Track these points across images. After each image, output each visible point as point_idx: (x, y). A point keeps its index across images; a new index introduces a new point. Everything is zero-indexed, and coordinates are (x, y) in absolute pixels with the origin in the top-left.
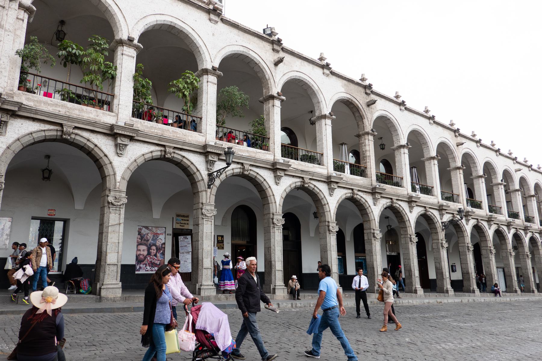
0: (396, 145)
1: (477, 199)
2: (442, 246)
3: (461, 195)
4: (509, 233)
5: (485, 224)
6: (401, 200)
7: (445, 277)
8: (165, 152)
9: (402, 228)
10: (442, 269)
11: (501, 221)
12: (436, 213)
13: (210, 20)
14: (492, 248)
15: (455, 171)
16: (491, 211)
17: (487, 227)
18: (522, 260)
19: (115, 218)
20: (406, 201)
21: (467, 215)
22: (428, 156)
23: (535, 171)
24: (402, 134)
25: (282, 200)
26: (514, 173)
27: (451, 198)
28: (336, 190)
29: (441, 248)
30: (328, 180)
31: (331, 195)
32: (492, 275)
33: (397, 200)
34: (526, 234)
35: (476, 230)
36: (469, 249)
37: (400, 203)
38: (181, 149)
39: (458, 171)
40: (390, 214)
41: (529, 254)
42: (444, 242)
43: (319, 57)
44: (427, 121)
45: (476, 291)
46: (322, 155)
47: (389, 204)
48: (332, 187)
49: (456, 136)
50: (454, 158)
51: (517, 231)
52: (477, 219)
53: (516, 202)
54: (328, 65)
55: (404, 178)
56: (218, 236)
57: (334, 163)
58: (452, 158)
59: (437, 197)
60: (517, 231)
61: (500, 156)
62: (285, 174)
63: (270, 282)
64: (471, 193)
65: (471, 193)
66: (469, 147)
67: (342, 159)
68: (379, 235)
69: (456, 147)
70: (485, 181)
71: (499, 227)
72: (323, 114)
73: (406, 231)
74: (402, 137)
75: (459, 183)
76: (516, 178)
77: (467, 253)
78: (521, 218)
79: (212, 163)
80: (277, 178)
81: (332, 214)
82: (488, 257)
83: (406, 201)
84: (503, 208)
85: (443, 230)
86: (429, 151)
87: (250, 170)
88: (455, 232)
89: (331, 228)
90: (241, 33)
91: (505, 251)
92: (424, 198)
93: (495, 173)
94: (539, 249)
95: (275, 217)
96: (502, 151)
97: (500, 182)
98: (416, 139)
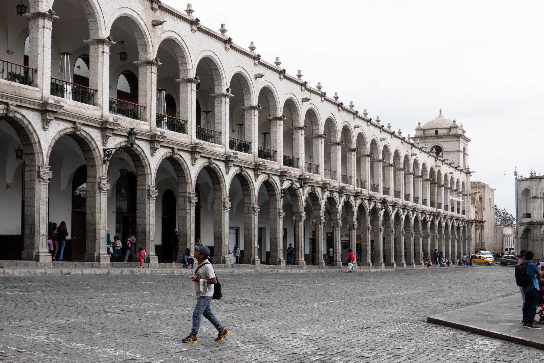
0: (32, 11)
2: (225, 207)
3: (148, 107)
4: (227, 173)
5: (221, 166)
6: (28, 108)
7: (98, 237)
9: (28, 154)
10: (95, 224)
11: (214, 154)
12: (95, 135)
14: (153, 189)
15: (144, 68)
16: (198, 137)
18: (246, 216)
20: (37, 110)
22: (95, 38)
23: (291, 80)
24: (191, 63)
26: (253, 79)
29: (97, 191)
30: (42, 107)
31: (193, 165)
32: (186, 236)
33: (18, 106)
34: (257, 176)
35: (266, 187)
36: (254, 211)
37: (24, 112)
39: (149, 67)
40: (170, 168)
41: (256, 206)
42: (227, 201)
44: (299, 86)
45: (256, 262)
46: (36, 71)
47: (168, 155)
48: (48, 117)
49: (152, 8)
50: (145, 45)
51: (242, 170)
52: (173, 149)
53: (250, 126)
55: (39, 71)
56: (327, 233)
57: (52, 84)
58: (142, 45)
59: (101, 107)
60: (242, 170)
61: (232, 51)
62: (113, 134)
65: (172, 104)
66: (271, 79)
67: (63, 76)
68: (106, 185)
69: (150, 27)
70: (325, 141)
71: (210, 163)
72: (189, 77)
73: (33, 160)
74: (151, 50)
75: (149, 88)
76: (303, 109)
77: (147, 201)
78: (253, 151)
80: (46, 122)
81: (45, 157)
82: (185, 209)
83: (147, 141)
84: (320, 167)
85: (105, 162)
86: (97, 29)
87: (16, 112)
88: (175, 176)
89: (41, 174)
91: (274, 210)
92: (172, 135)
93: (219, 77)
94: (276, 201)
95: (41, 170)
96: (288, 73)
97: (224, 91)
98: (208, 68)
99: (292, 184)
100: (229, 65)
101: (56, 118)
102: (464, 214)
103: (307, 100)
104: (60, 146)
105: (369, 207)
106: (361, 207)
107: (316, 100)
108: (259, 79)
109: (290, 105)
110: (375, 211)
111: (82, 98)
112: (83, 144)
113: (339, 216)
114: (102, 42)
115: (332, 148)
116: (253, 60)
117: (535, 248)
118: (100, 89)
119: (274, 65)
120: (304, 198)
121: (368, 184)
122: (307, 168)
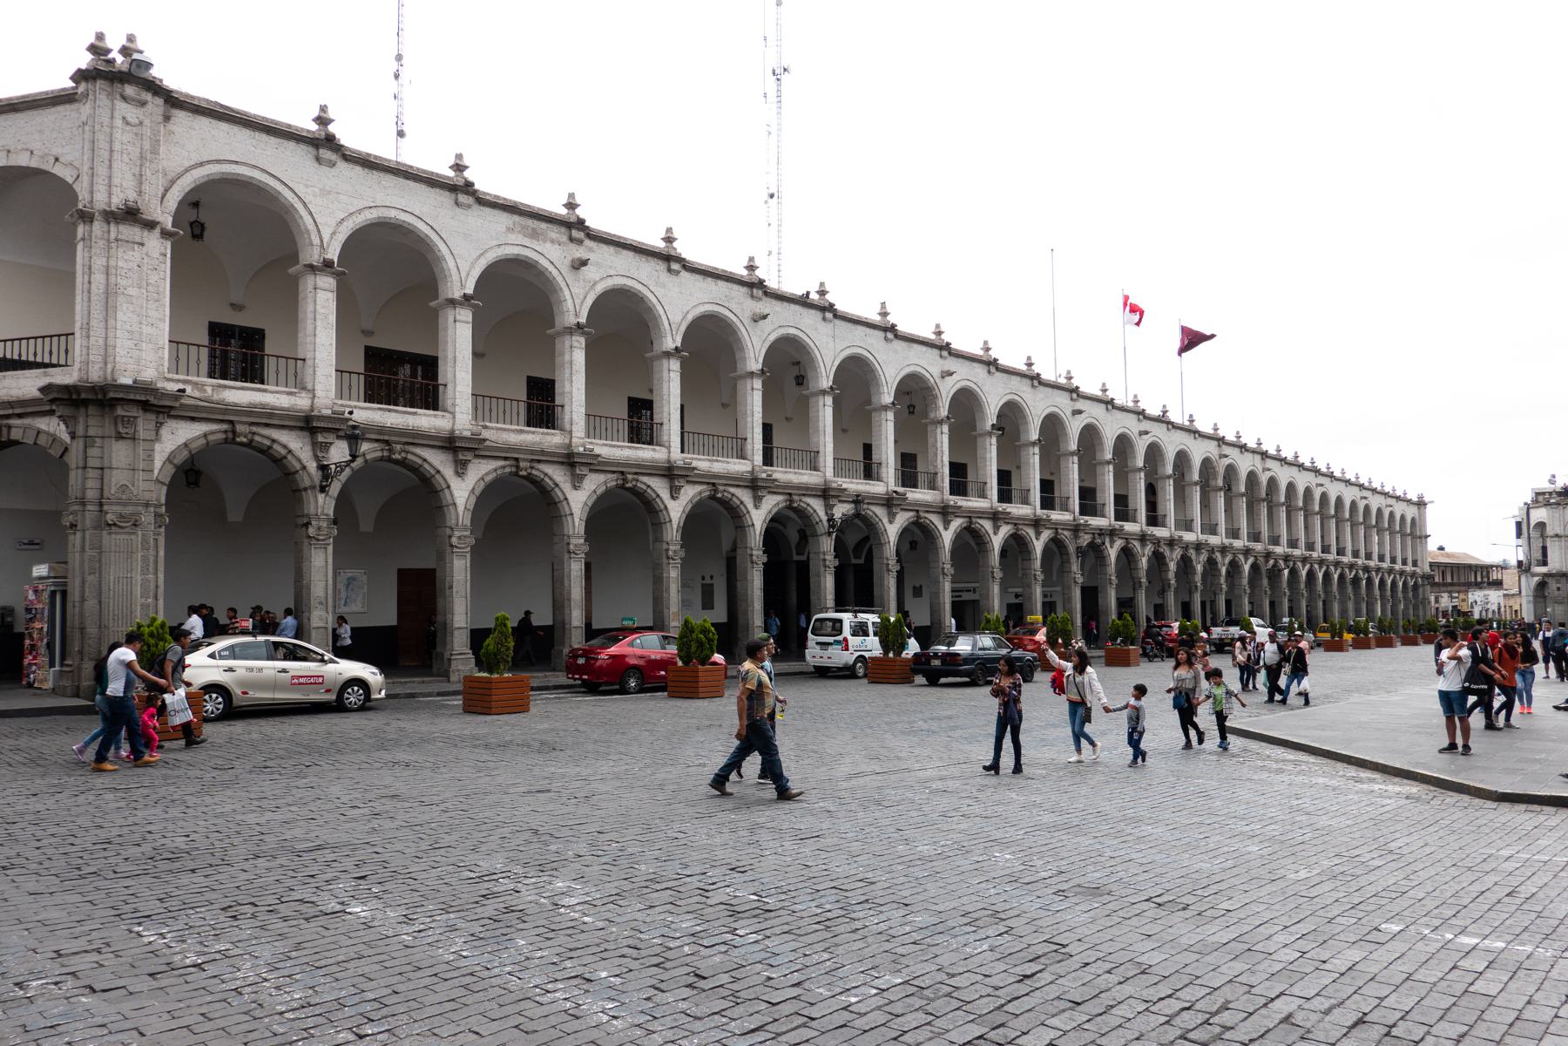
1: (1160, 512)
5: (1031, 532)
8: (234, 432)
13: (318, 159)
14: (948, 566)
17: (664, 494)
19: (320, 562)
21: (946, 512)
23: (1123, 409)
25: (473, 500)
27: (1211, 529)
28: (470, 466)
38: (267, 425)
43: (452, 162)
54: (893, 326)
63: (445, 644)
64: (1152, 505)
66: (1094, 413)
76: (1074, 428)
79: (326, 447)
81: (577, 521)
90: (967, 363)
99: (918, 517)
100: (1037, 406)
101: (477, 456)
102: (1415, 564)
103: (1146, 433)
104: (695, 517)
105: (1350, 575)
106: (1342, 577)
107: (1233, 453)
108: (948, 379)
109: (1123, 443)
110: (1356, 581)
111: (388, 395)
112: (802, 514)
113: (1223, 580)
114: (824, 392)
115: (1212, 495)
116: (311, 149)
117: (113, 574)
118: (749, 436)
119: (876, 318)
120: (1144, 560)
121: (1302, 543)
122: (1082, 513)
